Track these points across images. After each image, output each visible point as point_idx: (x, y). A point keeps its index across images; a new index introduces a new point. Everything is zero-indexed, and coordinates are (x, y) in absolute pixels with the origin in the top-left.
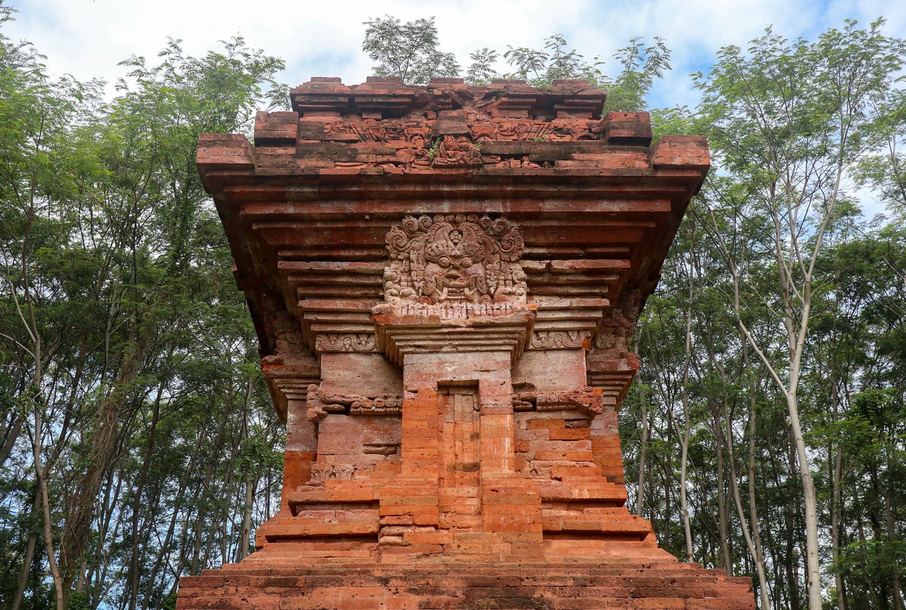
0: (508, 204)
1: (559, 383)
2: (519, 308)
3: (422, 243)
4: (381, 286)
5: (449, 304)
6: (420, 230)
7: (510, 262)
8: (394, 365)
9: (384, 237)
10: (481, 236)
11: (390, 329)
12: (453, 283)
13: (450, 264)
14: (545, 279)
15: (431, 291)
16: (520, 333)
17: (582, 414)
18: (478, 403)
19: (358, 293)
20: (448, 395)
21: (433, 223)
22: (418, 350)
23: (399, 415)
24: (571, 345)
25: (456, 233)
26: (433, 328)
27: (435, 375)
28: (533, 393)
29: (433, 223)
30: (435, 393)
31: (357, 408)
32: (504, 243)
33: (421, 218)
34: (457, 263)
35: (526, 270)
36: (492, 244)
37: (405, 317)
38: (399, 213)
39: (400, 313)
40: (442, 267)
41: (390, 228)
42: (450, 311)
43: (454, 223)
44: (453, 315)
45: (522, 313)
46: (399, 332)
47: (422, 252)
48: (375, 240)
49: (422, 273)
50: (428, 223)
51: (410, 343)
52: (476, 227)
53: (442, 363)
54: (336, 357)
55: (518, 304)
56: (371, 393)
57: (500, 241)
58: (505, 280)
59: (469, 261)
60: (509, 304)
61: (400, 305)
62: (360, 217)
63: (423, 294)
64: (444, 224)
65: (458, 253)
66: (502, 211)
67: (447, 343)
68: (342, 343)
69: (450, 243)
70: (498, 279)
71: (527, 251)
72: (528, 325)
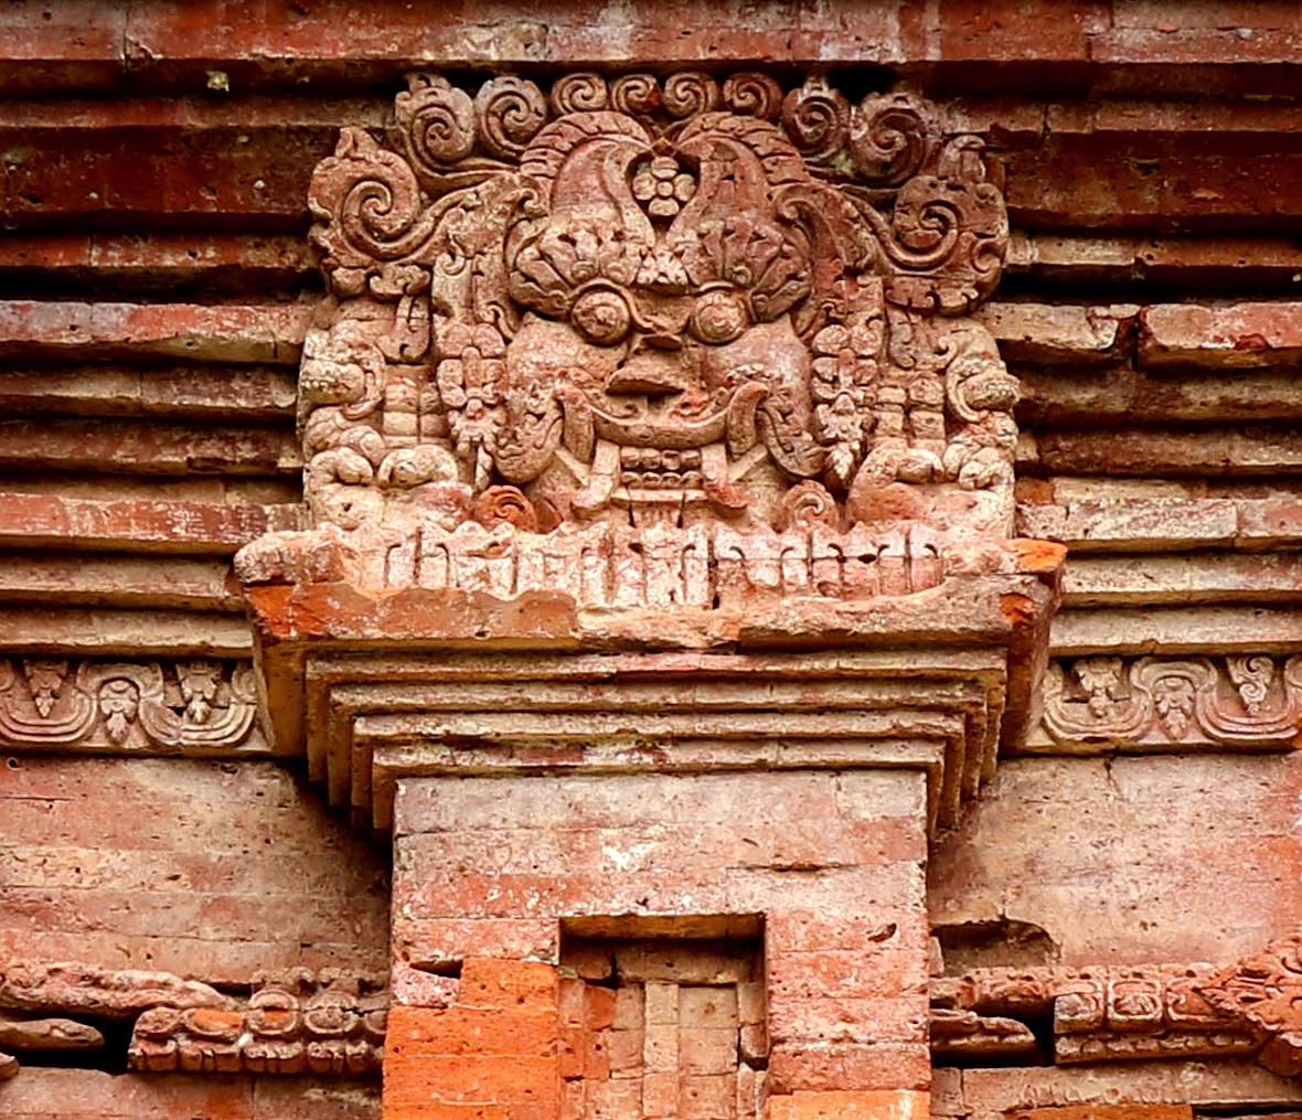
0: (931, 20)
1: (1171, 926)
2: (971, 560)
3: (494, 220)
4: (284, 426)
5: (623, 532)
6: (481, 147)
7: (935, 313)
8: (350, 826)
9: (304, 183)
10: (794, 186)
11: (327, 656)
12: (647, 420)
13: (633, 327)
14: (1113, 398)
15: (534, 460)
16: (972, 683)
17: (1281, 1078)
18: (761, 1026)
19: (171, 457)
20: (614, 982)
21: (552, 114)
22: (465, 760)
23: (369, 1077)
24: (1238, 728)
25: (665, 167)
26: (539, 655)
27: (547, 887)
28: (1038, 972)
29: (552, 114)
30: (550, 979)
31: (161, 1039)
32: (906, 220)
33: (489, 90)
34: (667, 322)
35: (1018, 356)
36: (844, 225)
37: (403, 600)
38: (377, 63)
39: (376, 575)
40: (589, 339)
41: (335, 135)
42: (628, 568)
43: (656, 114)
44: (642, 585)
45: (987, 585)
46: (369, 669)
47: (490, 263)
48: (257, 193)
49: (489, 368)
50: (520, 118)
51: (428, 726)
52: (767, 138)
53: (583, 827)
54: (62, 778)
55: (966, 534)
56: (231, 959)
57: (885, 205)
58: (908, 408)
59: (724, 310)
60: (922, 535)
61: (378, 535)
62: (184, 80)
63: (496, 476)
64: (605, 119)
65: (675, 272)
66: (896, 54)
67: (611, 725)
68: (88, 710)
69: (635, 220)
70: (872, 404)
71: (1028, 254)
72: (1015, 644)
